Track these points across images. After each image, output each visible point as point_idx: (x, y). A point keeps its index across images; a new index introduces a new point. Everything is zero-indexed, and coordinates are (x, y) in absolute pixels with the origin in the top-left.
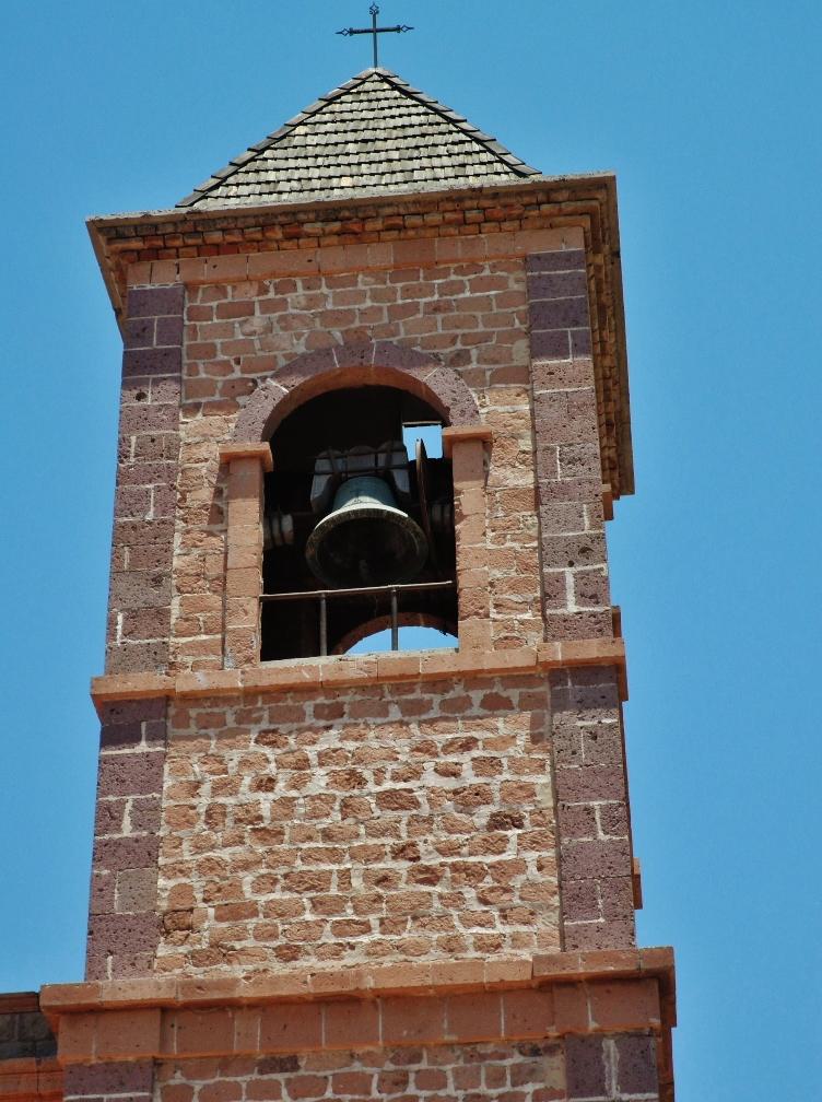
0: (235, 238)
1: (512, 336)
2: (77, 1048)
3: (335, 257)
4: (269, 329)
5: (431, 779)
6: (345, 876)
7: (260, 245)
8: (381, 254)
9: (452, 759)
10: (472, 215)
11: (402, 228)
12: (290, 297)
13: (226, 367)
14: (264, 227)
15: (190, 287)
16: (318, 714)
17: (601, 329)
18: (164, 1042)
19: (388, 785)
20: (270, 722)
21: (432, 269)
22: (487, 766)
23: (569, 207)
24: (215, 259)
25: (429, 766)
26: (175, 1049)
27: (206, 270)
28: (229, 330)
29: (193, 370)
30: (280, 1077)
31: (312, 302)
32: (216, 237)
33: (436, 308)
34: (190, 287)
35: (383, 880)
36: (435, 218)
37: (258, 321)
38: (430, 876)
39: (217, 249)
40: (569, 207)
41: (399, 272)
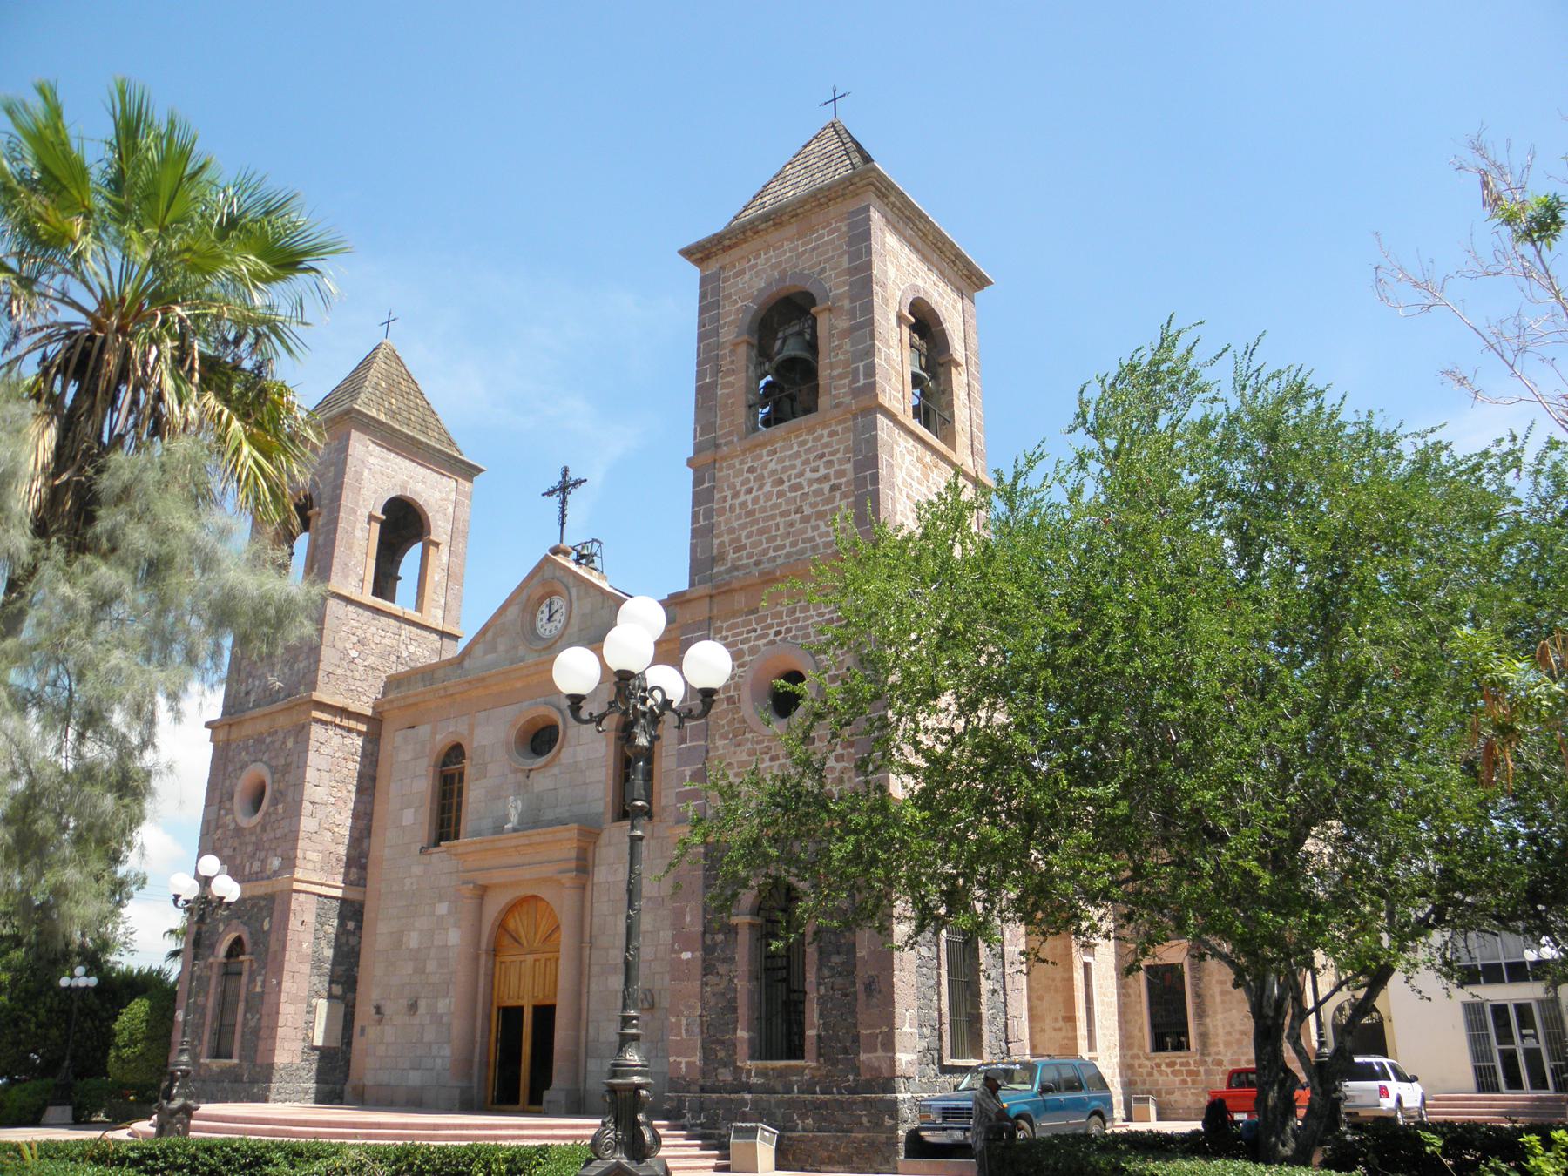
0: (734, 241)
1: (841, 256)
2: (440, 674)
3: (773, 236)
4: (751, 279)
5: (808, 475)
6: (777, 525)
7: (745, 240)
8: (790, 230)
9: (816, 464)
10: (822, 200)
11: (797, 215)
12: (759, 261)
13: (735, 302)
14: (744, 232)
15: (722, 268)
16: (768, 455)
17: (915, 225)
18: (711, 610)
19: (793, 481)
20: (375, 593)
21: (813, 230)
22: (830, 464)
23: (861, 184)
24: (731, 252)
25: (808, 470)
26: (715, 612)
27: (726, 259)
28: (736, 284)
29: (724, 307)
30: (752, 617)
31: (767, 260)
32: (727, 242)
33: (813, 249)
34: (722, 268)
35: (792, 525)
36: (808, 207)
37: (747, 276)
38: (806, 519)
39: (730, 247)
40: (861, 184)
41: (801, 235)
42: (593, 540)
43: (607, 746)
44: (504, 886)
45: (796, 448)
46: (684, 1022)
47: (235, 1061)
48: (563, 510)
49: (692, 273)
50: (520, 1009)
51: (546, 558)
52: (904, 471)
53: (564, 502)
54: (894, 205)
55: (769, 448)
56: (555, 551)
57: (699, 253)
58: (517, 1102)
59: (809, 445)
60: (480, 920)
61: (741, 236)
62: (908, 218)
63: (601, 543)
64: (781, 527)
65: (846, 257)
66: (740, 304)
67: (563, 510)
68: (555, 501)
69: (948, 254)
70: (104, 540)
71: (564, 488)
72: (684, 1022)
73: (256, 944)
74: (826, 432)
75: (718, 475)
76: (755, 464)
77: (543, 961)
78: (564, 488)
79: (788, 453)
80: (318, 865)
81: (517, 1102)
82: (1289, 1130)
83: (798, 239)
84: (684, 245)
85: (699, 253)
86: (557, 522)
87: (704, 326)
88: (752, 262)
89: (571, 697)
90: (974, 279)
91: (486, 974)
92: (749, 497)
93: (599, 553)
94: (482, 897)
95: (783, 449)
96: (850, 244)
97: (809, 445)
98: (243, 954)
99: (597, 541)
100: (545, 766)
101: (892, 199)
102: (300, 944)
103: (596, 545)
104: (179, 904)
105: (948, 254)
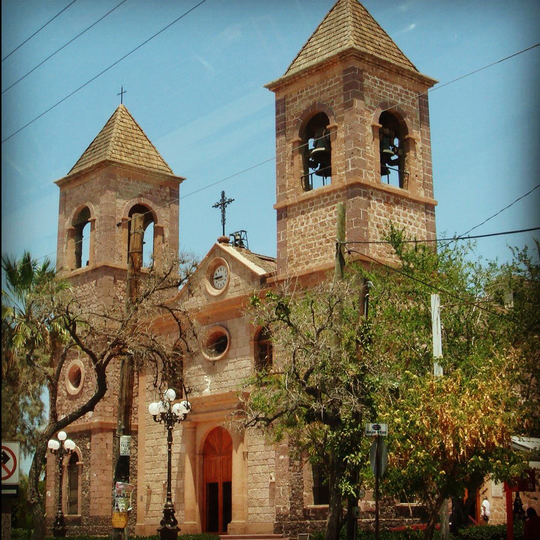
1: (340, 96)
5: (328, 218)
7: (295, 81)
19: (322, 221)
32: (287, 83)
39: (288, 85)
42: (242, 231)
43: (251, 348)
44: (206, 422)
45: (322, 203)
46: (281, 488)
47: (79, 515)
48: (223, 216)
49: (271, 97)
50: (216, 485)
51: (216, 245)
52: (375, 213)
53: (224, 211)
54: (368, 62)
55: (311, 202)
56: (221, 241)
57: (276, 87)
58: (218, 531)
59: (328, 202)
60: (195, 440)
61: (293, 80)
62: (379, 65)
63: (245, 232)
64: (317, 245)
65: (342, 97)
66: (295, 118)
67: (223, 216)
68: (219, 211)
69: (407, 75)
70: (20, 343)
71: (223, 204)
72: (281, 488)
73: (84, 456)
74: (335, 195)
75: (288, 214)
76: (304, 210)
77: (226, 460)
78: (223, 204)
79: (319, 205)
80: (112, 414)
81: (218, 531)
82: (172, 528)
83: (321, 83)
84: (269, 82)
85: (276, 87)
86: (220, 224)
87: (279, 130)
88: (300, 94)
89: (153, 416)
90: (426, 83)
91: (200, 468)
92: (303, 227)
93: (245, 239)
94: (195, 428)
95: (317, 203)
96: (344, 90)
97: (328, 202)
98: (78, 461)
99: (244, 231)
100: (221, 359)
101: (367, 59)
102: (106, 456)
103: (243, 233)
104: (53, 452)
105: (407, 75)
